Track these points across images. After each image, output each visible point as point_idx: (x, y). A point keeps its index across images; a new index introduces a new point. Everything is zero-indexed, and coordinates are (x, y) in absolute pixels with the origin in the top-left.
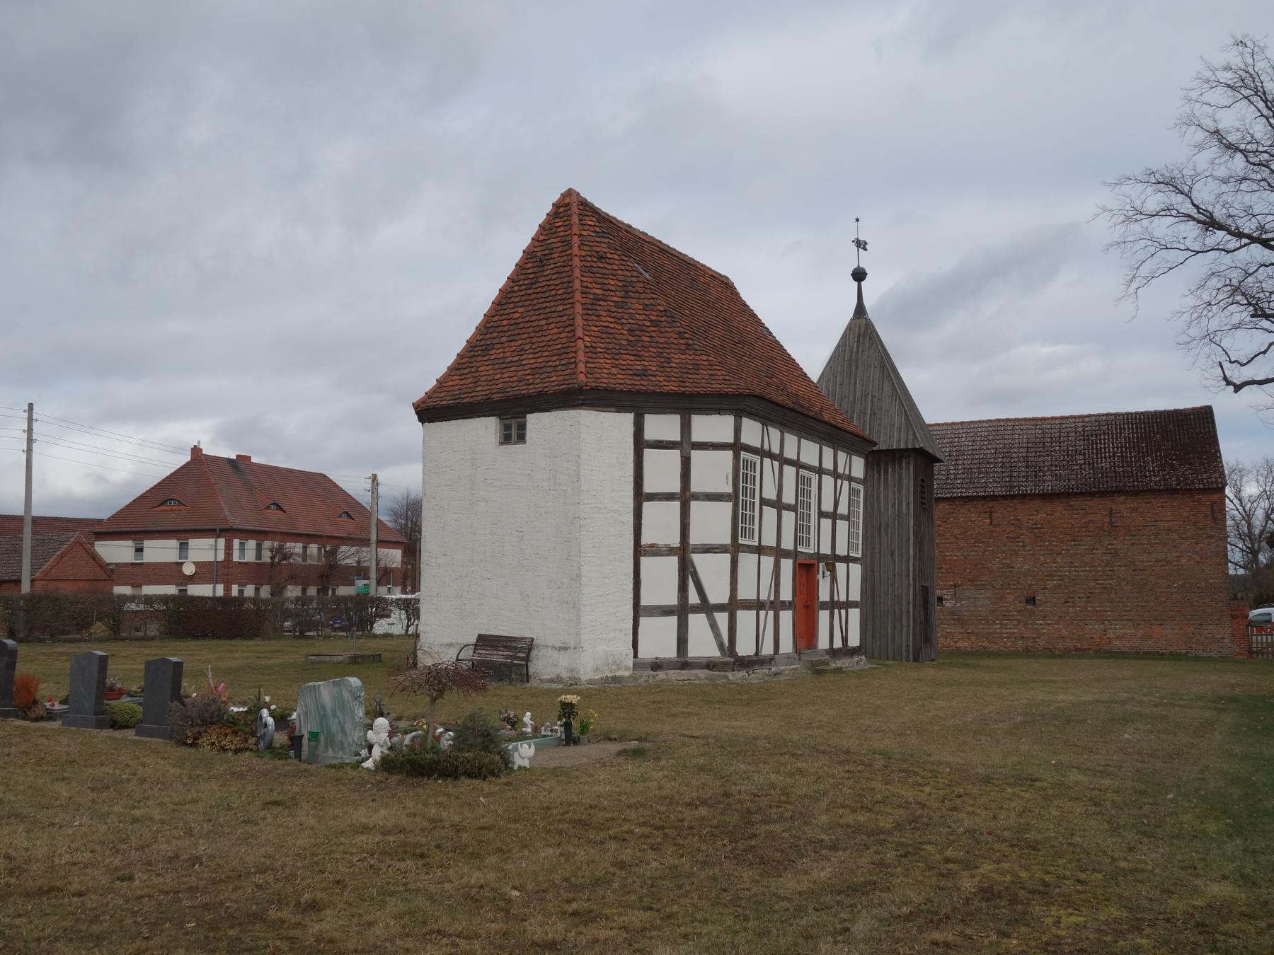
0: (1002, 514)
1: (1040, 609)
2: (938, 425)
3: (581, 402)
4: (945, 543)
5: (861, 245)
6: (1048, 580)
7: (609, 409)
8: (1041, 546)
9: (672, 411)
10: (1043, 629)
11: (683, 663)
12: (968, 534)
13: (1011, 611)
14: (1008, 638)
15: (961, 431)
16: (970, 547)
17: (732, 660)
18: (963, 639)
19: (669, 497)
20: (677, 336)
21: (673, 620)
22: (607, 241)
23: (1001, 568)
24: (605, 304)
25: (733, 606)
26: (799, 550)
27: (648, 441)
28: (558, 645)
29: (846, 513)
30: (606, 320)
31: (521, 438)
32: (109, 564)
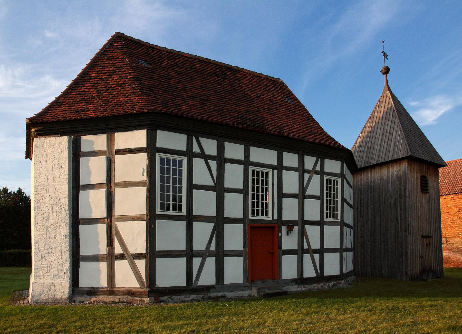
5: (386, 56)
25: (322, 251)
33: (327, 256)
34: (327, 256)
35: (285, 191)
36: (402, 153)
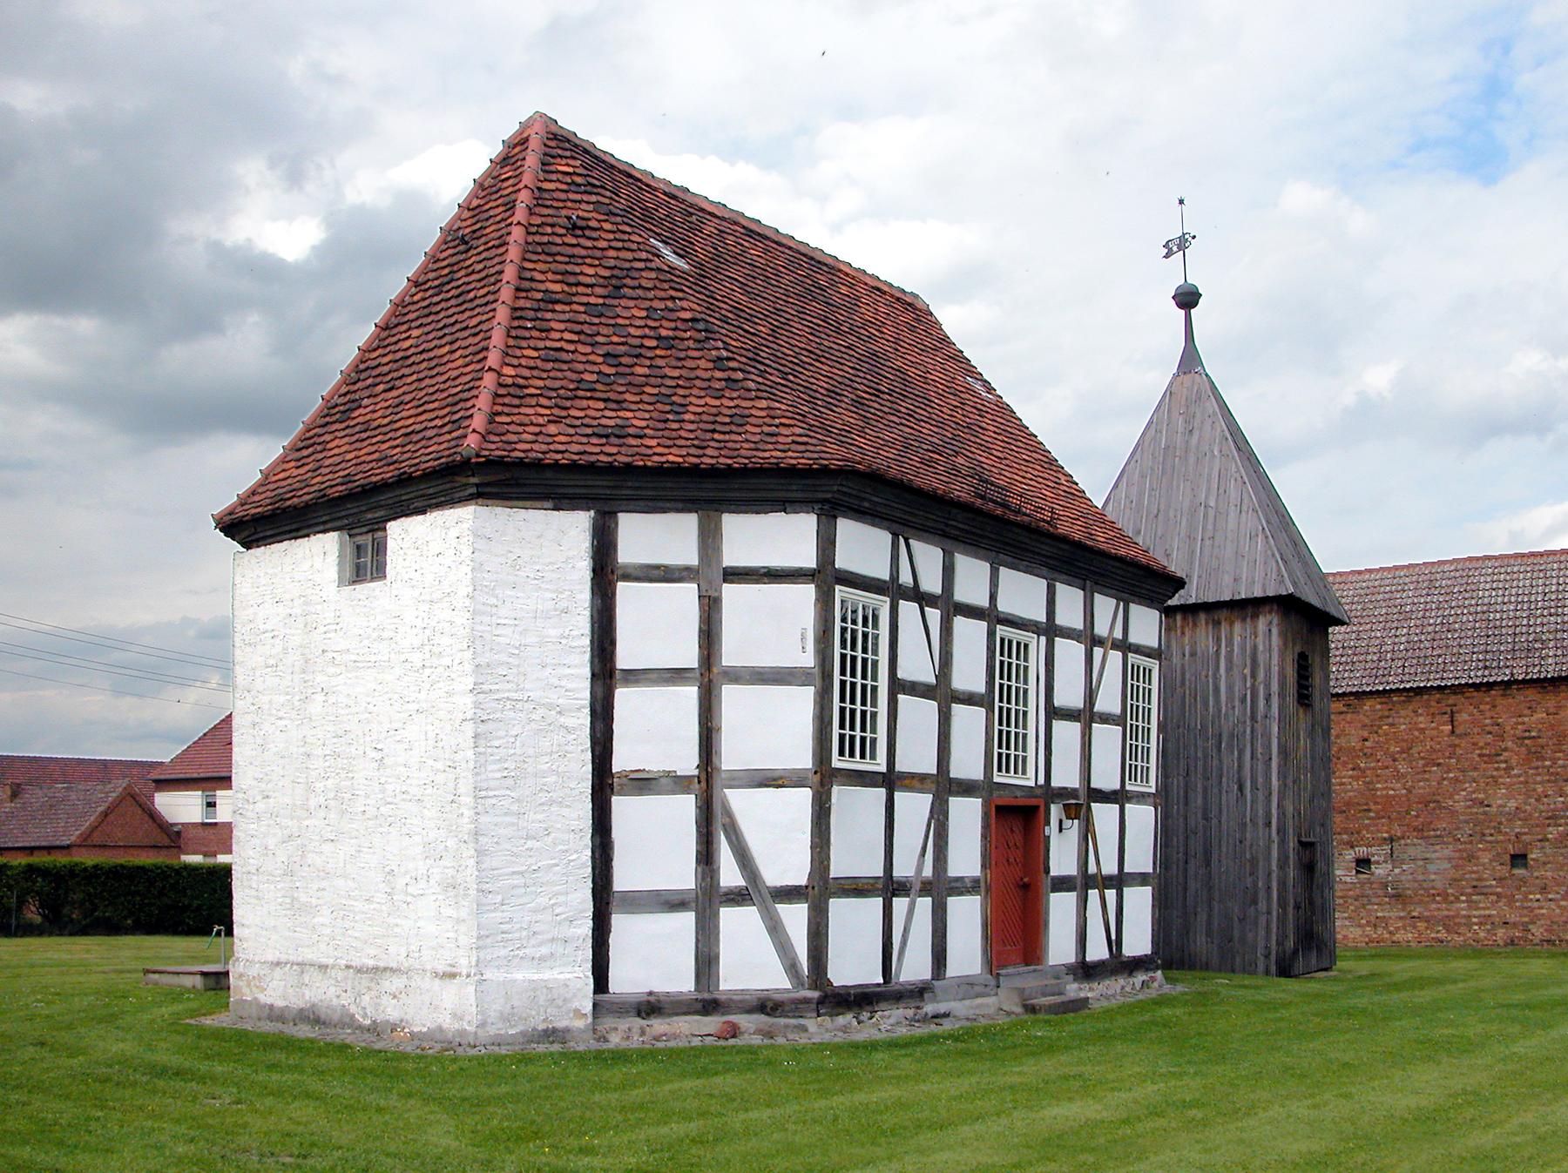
0: (1471, 714)
1: (1536, 874)
2: (1370, 571)
3: (474, 490)
4: (1374, 768)
6: (1549, 825)
7: (538, 504)
8: (1537, 768)
9: (680, 505)
10: (1542, 908)
11: (708, 1004)
12: (1414, 751)
13: (1486, 880)
14: (1480, 924)
15: (1407, 580)
16: (1418, 773)
17: (815, 994)
18: (1404, 927)
19: (675, 676)
20: (711, 365)
21: (687, 920)
22: (594, 198)
23: (1469, 807)
24: (567, 308)
26: (1128, 787)
27: (626, 566)
28: (441, 968)
29: (1117, 710)
30: (560, 334)
31: (379, 572)
32: (172, 825)
33: (840, 909)
34: (840, 909)
36: (1258, 575)
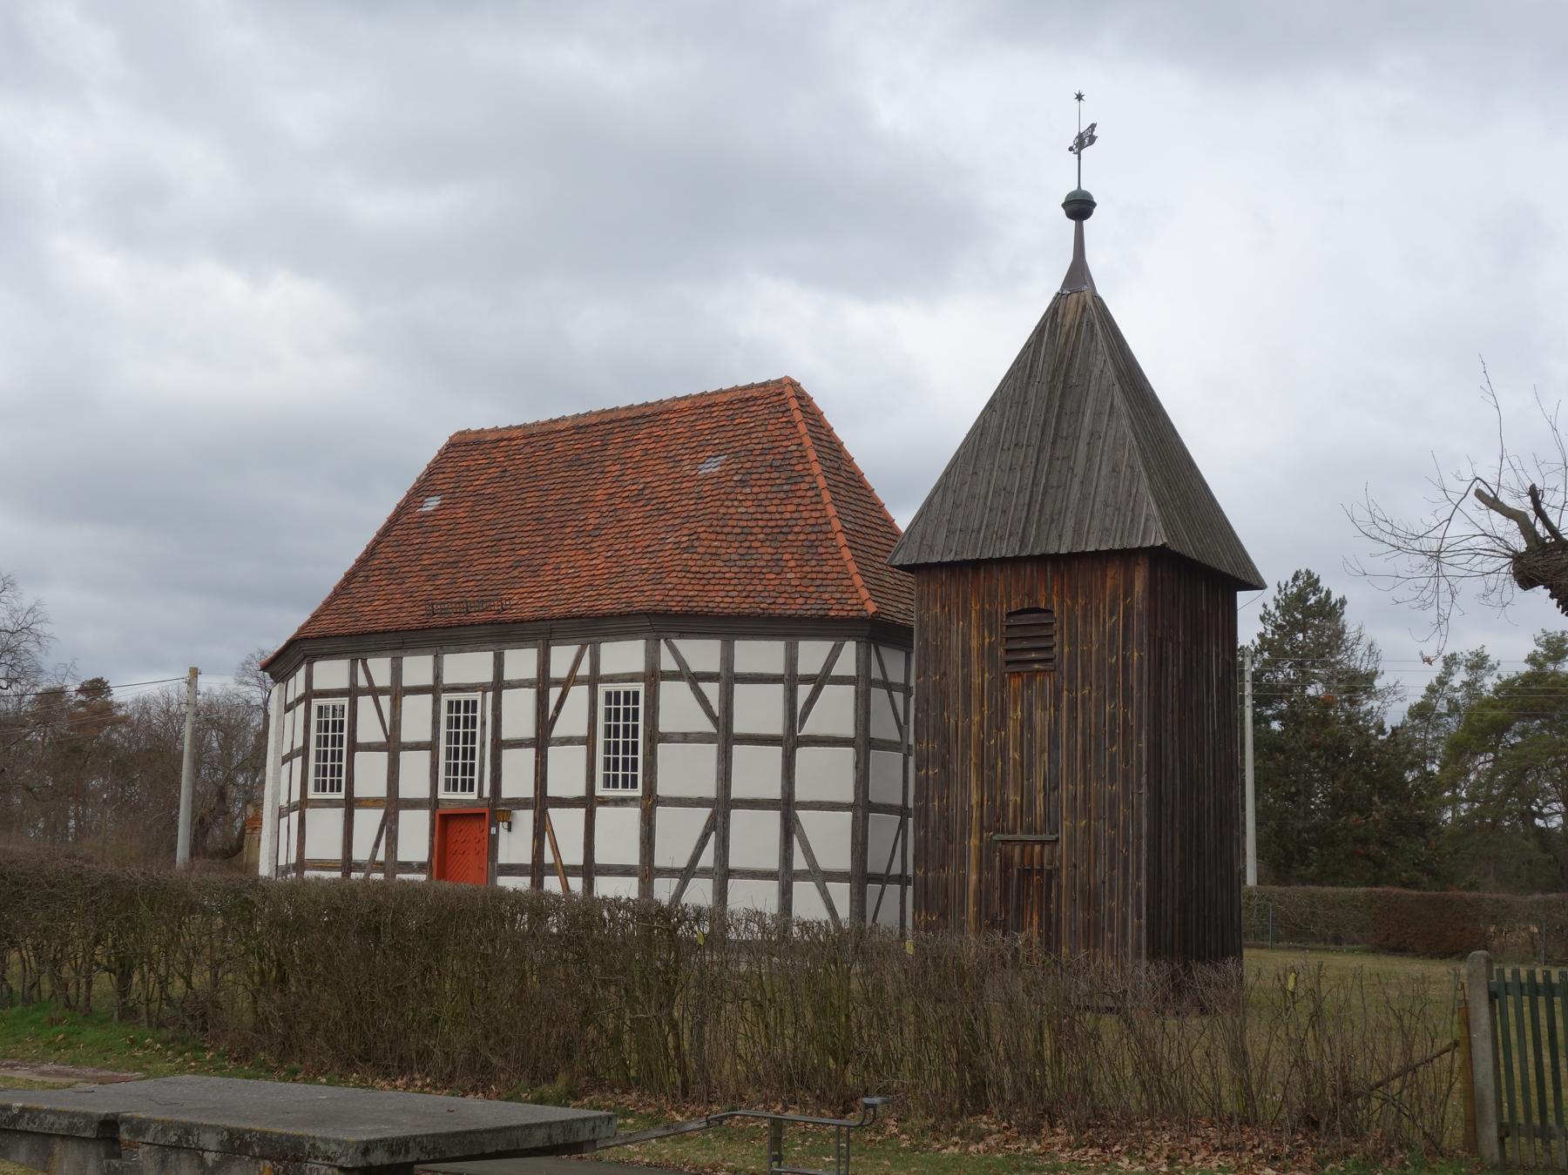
35: (506, 735)
